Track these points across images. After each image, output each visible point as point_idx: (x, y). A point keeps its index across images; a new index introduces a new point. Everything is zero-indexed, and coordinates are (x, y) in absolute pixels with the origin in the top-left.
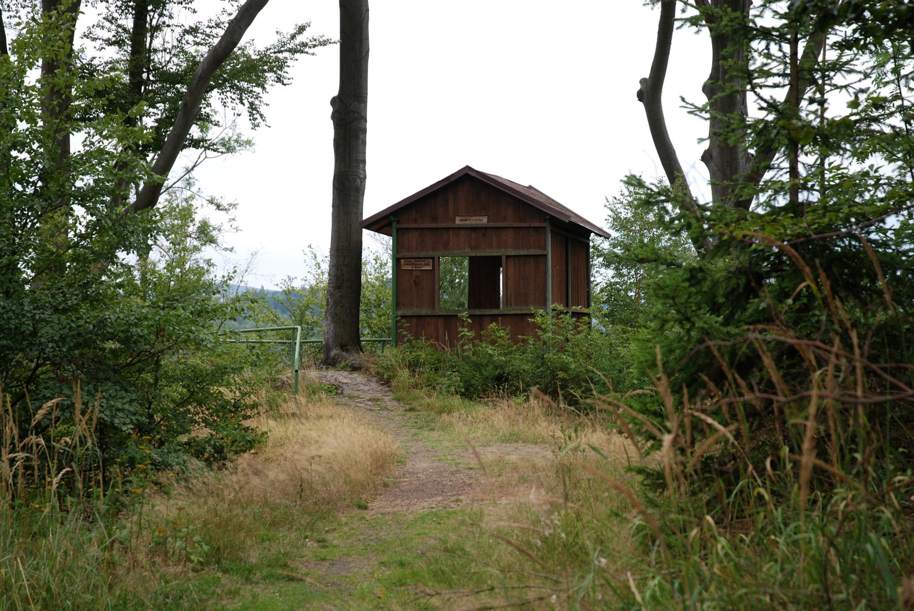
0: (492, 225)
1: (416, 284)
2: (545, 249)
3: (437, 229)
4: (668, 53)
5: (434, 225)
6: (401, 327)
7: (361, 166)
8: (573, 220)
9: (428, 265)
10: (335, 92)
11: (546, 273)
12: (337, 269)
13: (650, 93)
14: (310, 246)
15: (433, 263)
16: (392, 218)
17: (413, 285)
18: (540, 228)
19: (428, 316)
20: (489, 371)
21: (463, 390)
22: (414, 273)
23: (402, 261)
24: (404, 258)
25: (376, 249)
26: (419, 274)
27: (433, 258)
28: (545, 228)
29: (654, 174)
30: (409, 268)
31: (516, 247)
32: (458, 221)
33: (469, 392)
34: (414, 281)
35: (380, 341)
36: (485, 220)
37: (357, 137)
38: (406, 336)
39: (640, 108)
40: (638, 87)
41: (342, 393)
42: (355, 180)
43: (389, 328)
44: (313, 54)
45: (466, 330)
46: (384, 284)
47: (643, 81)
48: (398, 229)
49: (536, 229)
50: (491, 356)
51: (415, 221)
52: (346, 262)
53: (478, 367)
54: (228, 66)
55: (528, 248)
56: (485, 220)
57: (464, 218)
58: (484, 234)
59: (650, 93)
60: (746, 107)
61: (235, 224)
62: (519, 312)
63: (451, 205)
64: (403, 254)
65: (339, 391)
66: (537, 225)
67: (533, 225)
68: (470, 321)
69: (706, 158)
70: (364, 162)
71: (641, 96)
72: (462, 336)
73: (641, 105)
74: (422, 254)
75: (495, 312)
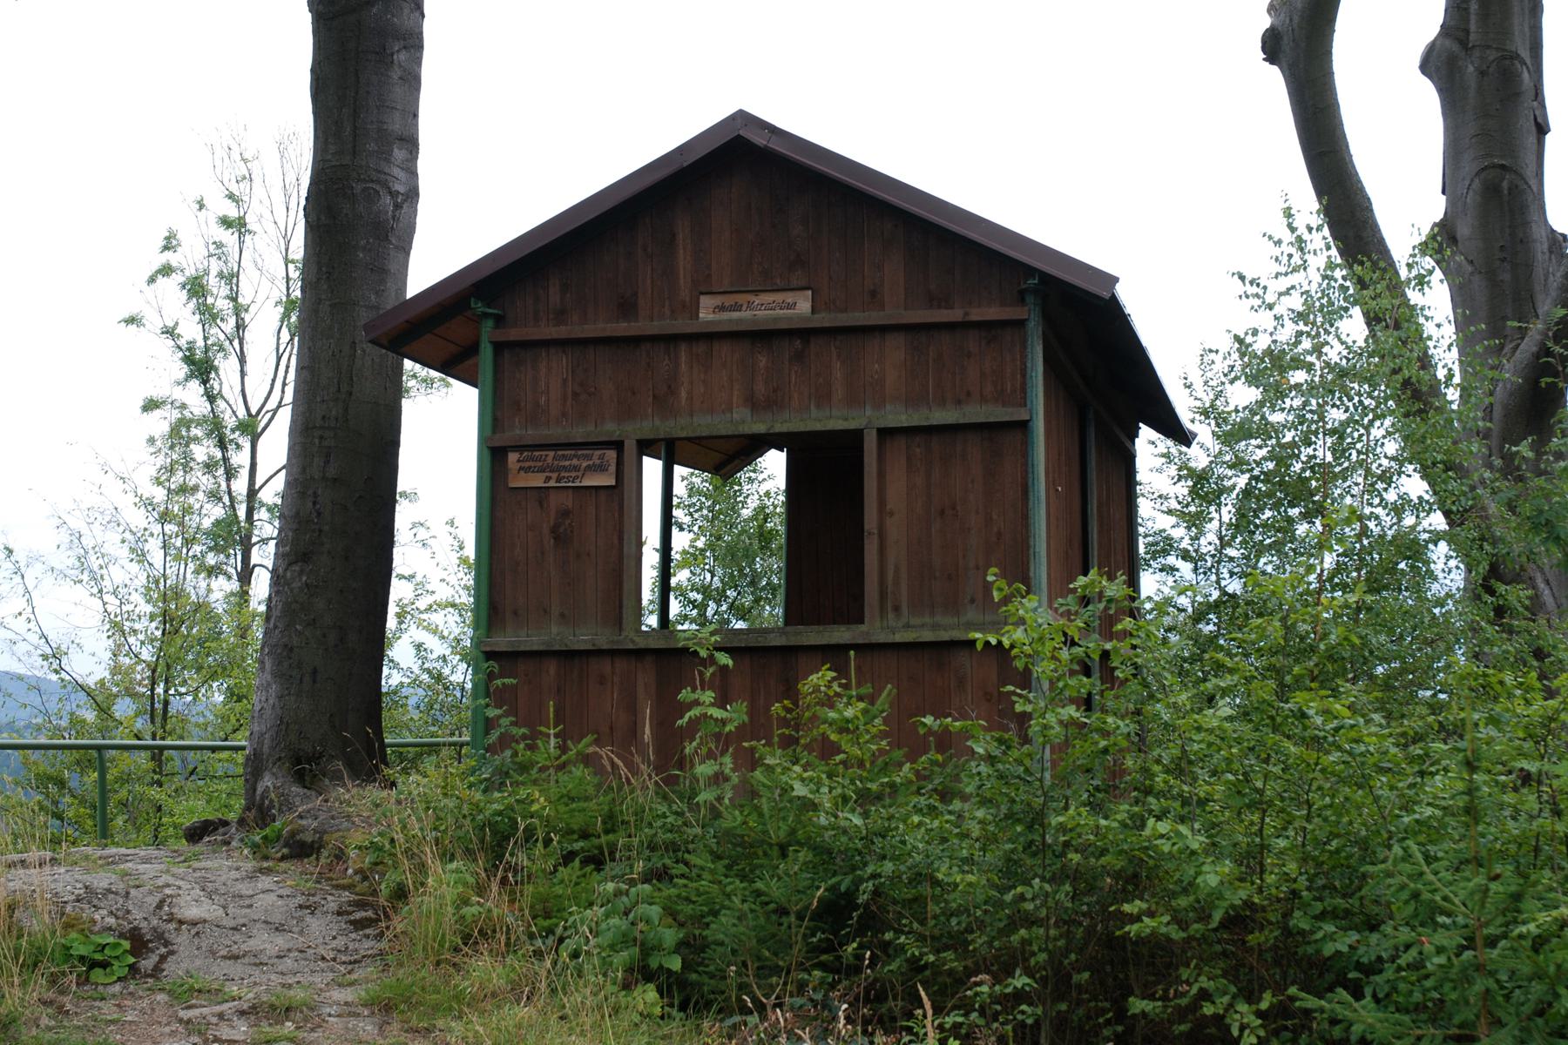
0: (825, 320)
1: (561, 537)
3: (636, 341)
5: (622, 328)
7: (399, 154)
9: (601, 468)
11: (1025, 491)
12: (302, 495)
14: (451, 523)
16: (479, 307)
17: (549, 542)
20: (787, 881)
21: (676, 964)
22: (555, 501)
23: (513, 457)
24: (519, 448)
25: (440, 432)
26: (568, 501)
28: (1020, 324)
30: (537, 481)
31: (914, 400)
32: (708, 312)
34: (554, 530)
37: (384, 58)
39: (1273, 83)
41: (157, 971)
42: (371, 197)
45: (708, 696)
48: (499, 347)
49: (988, 327)
50: (810, 806)
51: (561, 316)
52: (332, 472)
53: (742, 855)
56: (802, 304)
57: (729, 300)
58: (799, 357)
61: (422, 534)
62: (927, 636)
63: (684, 260)
65: (148, 964)
66: (992, 313)
67: (976, 315)
68: (724, 659)
70: (411, 143)
71: (1273, 47)
72: (694, 724)
74: (579, 433)
75: (840, 634)
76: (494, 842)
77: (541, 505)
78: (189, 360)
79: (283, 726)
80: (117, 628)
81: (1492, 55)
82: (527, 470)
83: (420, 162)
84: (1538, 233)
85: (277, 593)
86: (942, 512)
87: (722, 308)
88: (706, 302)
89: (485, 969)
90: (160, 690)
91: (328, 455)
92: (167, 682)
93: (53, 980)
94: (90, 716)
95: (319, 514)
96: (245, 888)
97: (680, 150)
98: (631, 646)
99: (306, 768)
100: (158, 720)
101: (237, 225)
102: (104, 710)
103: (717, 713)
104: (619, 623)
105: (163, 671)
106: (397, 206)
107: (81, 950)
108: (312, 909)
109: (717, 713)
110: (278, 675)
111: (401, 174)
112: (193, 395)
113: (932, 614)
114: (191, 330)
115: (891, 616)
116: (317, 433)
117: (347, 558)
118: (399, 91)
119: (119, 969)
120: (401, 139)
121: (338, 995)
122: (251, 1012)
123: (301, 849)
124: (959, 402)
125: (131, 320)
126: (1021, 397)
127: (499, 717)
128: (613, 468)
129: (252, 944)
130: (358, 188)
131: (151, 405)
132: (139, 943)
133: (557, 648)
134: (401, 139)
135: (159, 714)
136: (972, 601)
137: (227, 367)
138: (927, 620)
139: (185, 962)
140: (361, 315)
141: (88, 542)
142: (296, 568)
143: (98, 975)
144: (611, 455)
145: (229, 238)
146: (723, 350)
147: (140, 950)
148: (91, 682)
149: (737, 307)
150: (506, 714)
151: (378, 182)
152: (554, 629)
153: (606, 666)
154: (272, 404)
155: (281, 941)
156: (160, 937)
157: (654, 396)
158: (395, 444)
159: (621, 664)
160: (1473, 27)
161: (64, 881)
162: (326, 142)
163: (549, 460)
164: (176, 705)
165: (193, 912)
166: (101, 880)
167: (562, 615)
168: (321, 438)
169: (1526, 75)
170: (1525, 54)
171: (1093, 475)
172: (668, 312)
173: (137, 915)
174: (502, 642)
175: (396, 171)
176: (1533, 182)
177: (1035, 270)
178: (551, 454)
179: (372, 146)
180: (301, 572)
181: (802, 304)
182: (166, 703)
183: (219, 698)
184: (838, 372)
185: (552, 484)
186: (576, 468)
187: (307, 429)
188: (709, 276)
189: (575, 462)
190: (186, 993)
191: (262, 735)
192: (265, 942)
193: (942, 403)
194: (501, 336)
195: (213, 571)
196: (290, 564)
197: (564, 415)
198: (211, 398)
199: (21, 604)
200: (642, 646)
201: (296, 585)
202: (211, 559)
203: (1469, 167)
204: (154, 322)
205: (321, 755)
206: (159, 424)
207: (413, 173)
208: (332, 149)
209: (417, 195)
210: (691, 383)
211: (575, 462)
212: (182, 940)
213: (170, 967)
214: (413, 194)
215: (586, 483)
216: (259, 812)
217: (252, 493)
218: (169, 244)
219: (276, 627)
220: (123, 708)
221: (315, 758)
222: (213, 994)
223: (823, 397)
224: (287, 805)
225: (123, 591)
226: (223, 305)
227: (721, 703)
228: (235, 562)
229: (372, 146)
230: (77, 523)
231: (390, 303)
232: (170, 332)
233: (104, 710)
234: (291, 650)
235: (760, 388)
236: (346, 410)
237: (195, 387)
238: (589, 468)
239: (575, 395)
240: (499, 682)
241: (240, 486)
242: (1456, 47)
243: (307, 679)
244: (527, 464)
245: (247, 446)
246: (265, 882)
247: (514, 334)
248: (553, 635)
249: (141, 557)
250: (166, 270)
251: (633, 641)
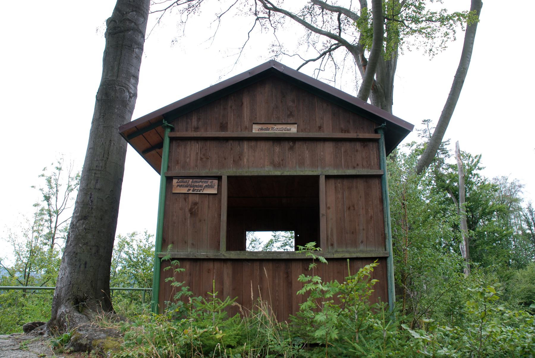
1: (193, 213)
6: (170, 273)
7: (132, 81)
9: (211, 187)
10: (109, 14)
12: (86, 194)
15: (219, 186)
16: (165, 123)
22: (191, 199)
23: (175, 181)
25: (141, 187)
26: (197, 199)
28: (377, 141)
30: (184, 190)
31: (337, 166)
32: (256, 130)
35: (143, 290)
37: (130, 48)
38: (179, 289)
42: (122, 92)
43: (150, 280)
46: (146, 251)
48: (172, 139)
49: (364, 141)
51: (197, 129)
52: (98, 186)
57: (264, 126)
63: (246, 112)
64: (177, 171)
66: (367, 136)
67: (362, 136)
72: (309, 293)
77: (185, 201)
78: (45, 197)
79: (71, 285)
80: (18, 253)
82: (181, 186)
83: (139, 87)
85: (72, 231)
86: (349, 208)
87: (262, 129)
90: (27, 270)
91: (97, 180)
92: (30, 268)
94: (8, 276)
95: (92, 202)
97: (249, 72)
98: (223, 258)
99: (79, 303)
100: (26, 278)
101: (60, 169)
102: (12, 276)
105: (29, 265)
106: (130, 97)
110: (70, 264)
111: (133, 87)
112: (45, 204)
113: (346, 247)
114: (46, 190)
115: (330, 247)
116: (93, 172)
117: (101, 219)
118: (135, 61)
120: (134, 76)
124: (354, 168)
125: (33, 187)
127: (180, 287)
128: (216, 187)
130: (118, 88)
131: (36, 205)
133: (191, 257)
134: (134, 76)
135: (27, 276)
136: (362, 242)
137: (53, 200)
138: (344, 249)
140: (116, 128)
142: (81, 222)
144: (216, 182)
145: (57, 172)
146: (262, 145)
148: (9, 267)
149: (268, 129)
150: (185, 285)
151: (125, 87)
152: (189, 250)
153: (211, 265)
154: (62, 208)
157: (234, 161)
158: (121, 180)
159: (217, 265)
162: (107, 75)
163: (190, 183)
164: (32, 274)
167: (193, 244)
168: (95, 173)
172: (240, 130)
175: (131, 86)
178: (191, 180)
179: (124, 75)
180: (83, 223)
181: (293, 130)
182: (29, 274)
183: (43, 273)
184: (307, 154)
185: (191, 192)
186: (201, 186)
187: (90, 170)
188: (256, 118)
189: (200, 184)
191: (61, 288)
193: (348, 167)
194: (173, 135)
195: (46, 244)
196: (79, 220)
197: (196, 166)
198: (49, 205)
200: (228, 257)
201: (81, 228)
202: (45, 241)
204: (38, 188)
205: (86, 298)
207: (136, 88)
208: (110, 75)
209: (136, 96)
210: (249, 156)
211: (200, 184)
214: (135, 95)
215: (205, 192)
217: (56, 227)
219: (71, 245)
221: (83, 299)
223: (301, 163)
225: (20, 244)
226: (54, 186)
228: (50, 243)
229: (124, 75)
232: (41, 190)
233: (12, 276)
234: (77, 254)
235: (276, 159)
236: (106, 164)
237: (46, 203)
238: (206, 186)
239: (201, 159)
240: (178, 270)
241: (53, 225)
243: (82, 266)
244: (181, 184)
245: (56, 216)
249: (26, 235)
251: (224, 255)
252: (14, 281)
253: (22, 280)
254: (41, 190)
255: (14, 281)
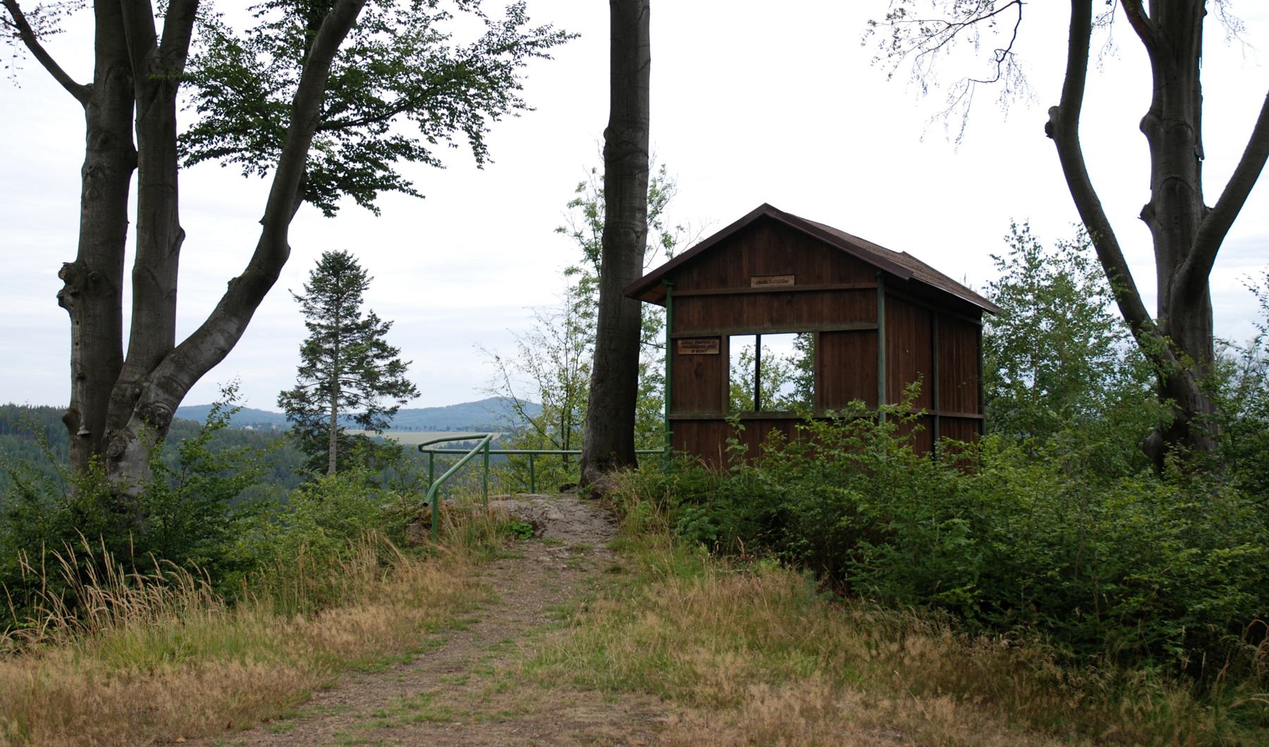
0: (800, 287)
2: (876, 322)
3: (727, 296)
4: (1085, 70)
7: (638, 215)
8: (917, 275)
9: (713, 347)
13: (1063, 125)
16: (665, 282)
18: (869, 289)
19: (713, 420)
23: (680, 342)
24: (682, 339)
27: (719, 338)
28: (875, 289)
29: (1059, 225)
30: (689, 352)
32: (754, 285)
33: (720, 547)
36: (791, 281)
37: (632, 177)
39: (1050, 148)
40: (1047, 118)
41: (541, 535)
44: (547, 56)
47: (1053, 111)
48: (674, 298)
54: (460, 88)
55: (851, 321)
57: (762, 279)
59: (1063, 125)
60: (1201, 147)
65: (538, 533)
66: (864, 285)
67: (858, 286)
68: (742, 427)
69: (1147, 214)
71: (1050, 130)
73: (1051, 143)
74: (705, 333)
76: (658, 493)
81: (1173, 123)
84: (1196, 209)
88: (754, 280)
89: (655, 539)
93: (507, 537)
94: (535, 434)
96: (573, 509)
102: (541, 432)
103: (739, 447)
104: (719, 407)
107: (515, 527)
108: (595, 516)
109: (739, 447)
119: (528, 534)
121: (600, 545)
122: (570, 550)
123: (596, 496)
125: (560, 230)
126: (875, 319)
129: (573, 528)
131: (570, 272)
132: (535, 526)
139: (550, 533)
141: (533, 353)
143: (521, 536)
144: (717, 341)
147: (535, 528)
152: (696, 411)
155: (583, 527)
156: (543, 525)
160: (1164, 109)
161: (512, 505)
165: (554, 516)
166: (524, 504)
169: (1190, 133)
170: (1190, 122)
171: (936, 341)
173: (535, 516)
174: (676, 416)
176: (1193, 186)
177: (879, 269)
190: (549, 543)
192: (578, 527)
199: (503, 382)
203: (1161, 178)
204: (571, 231)
206: (575, 280)
212: (549, 526)
213: (545, 534)
216: (584, 482)
218: (581, 188)
220: (550, 430)
222: (559, 544)
224: (593, 479)
227: (740, 443)
230: (528, 344)
231: (636, 278)
232: (578, 235)
242: (1155, 119)
246: (580, 507)
247: (679, 293)
248: (695, 413)
249: (556, 359)
250: (578, 203)
252: (547, 442)
253: (559, 439)
254: (578, 235)
255: (547, 442)
